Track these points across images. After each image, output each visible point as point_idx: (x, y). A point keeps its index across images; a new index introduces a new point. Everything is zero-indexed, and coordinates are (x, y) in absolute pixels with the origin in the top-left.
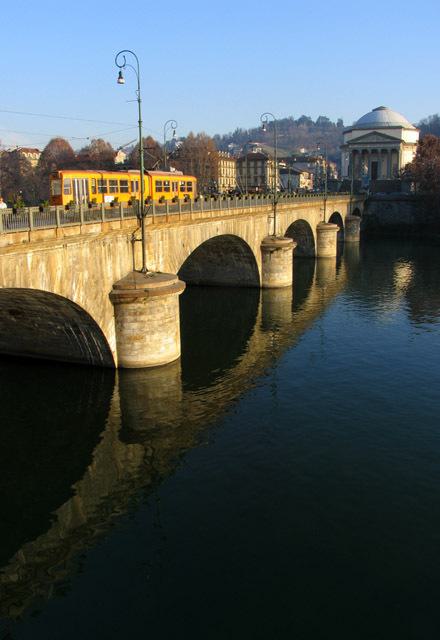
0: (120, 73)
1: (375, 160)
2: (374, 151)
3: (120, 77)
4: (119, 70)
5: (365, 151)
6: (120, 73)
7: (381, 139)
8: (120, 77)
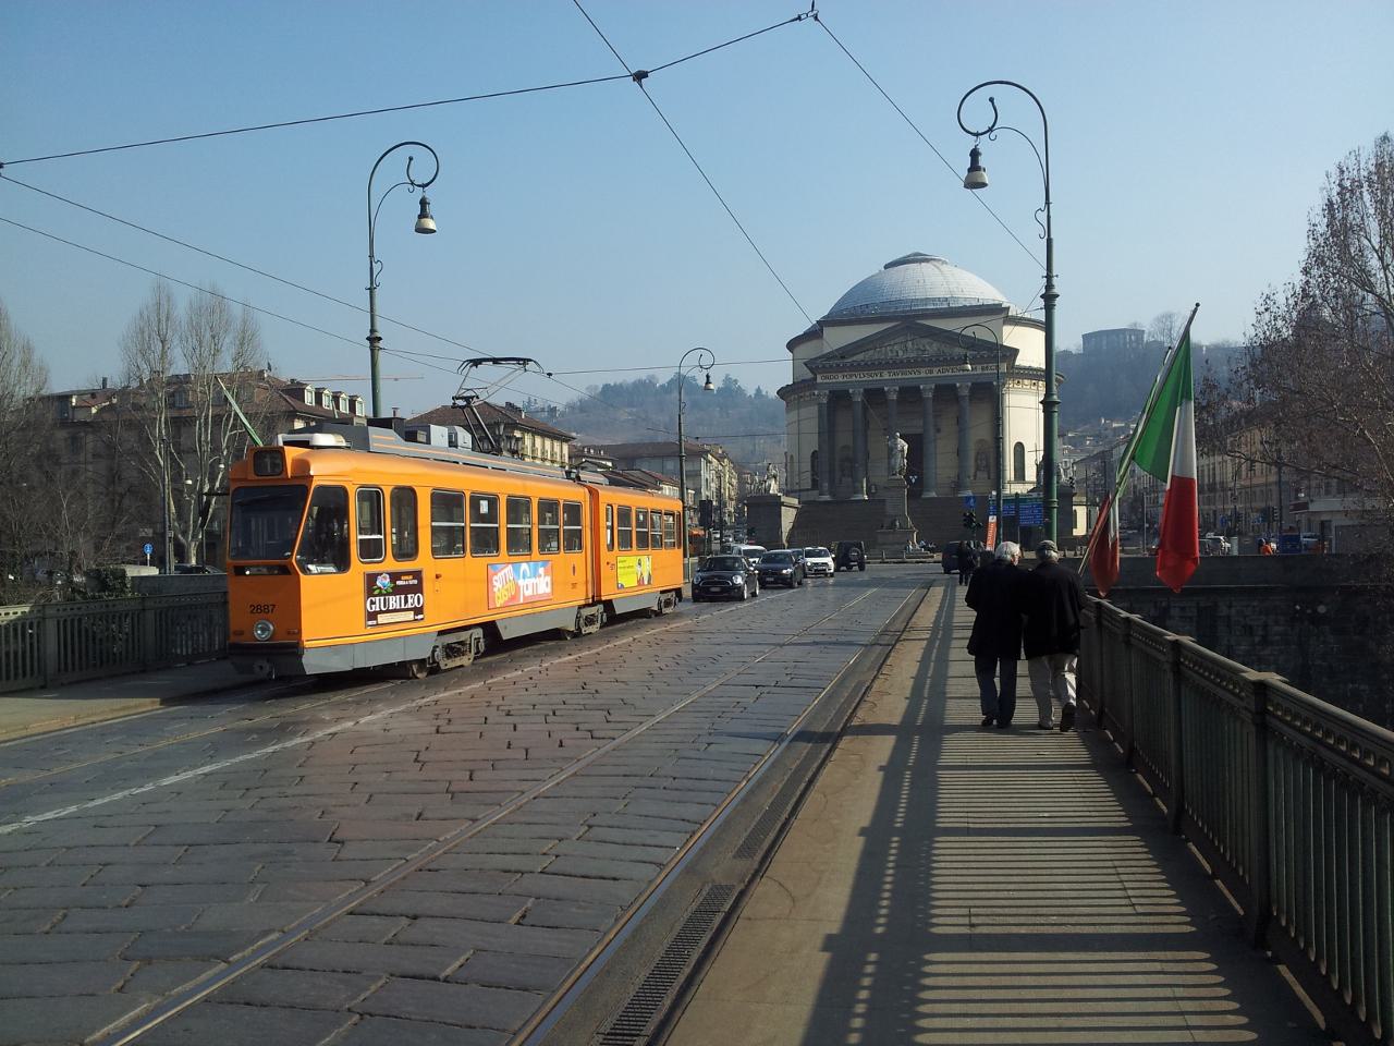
0: (975, 154)
1: (916, 427)
2: (910, 394)
3: (975, 167)
4: (970, 142)
5: (875, 395)
6: (975, 154)
7: (932, 348)
8: (975, 167)
